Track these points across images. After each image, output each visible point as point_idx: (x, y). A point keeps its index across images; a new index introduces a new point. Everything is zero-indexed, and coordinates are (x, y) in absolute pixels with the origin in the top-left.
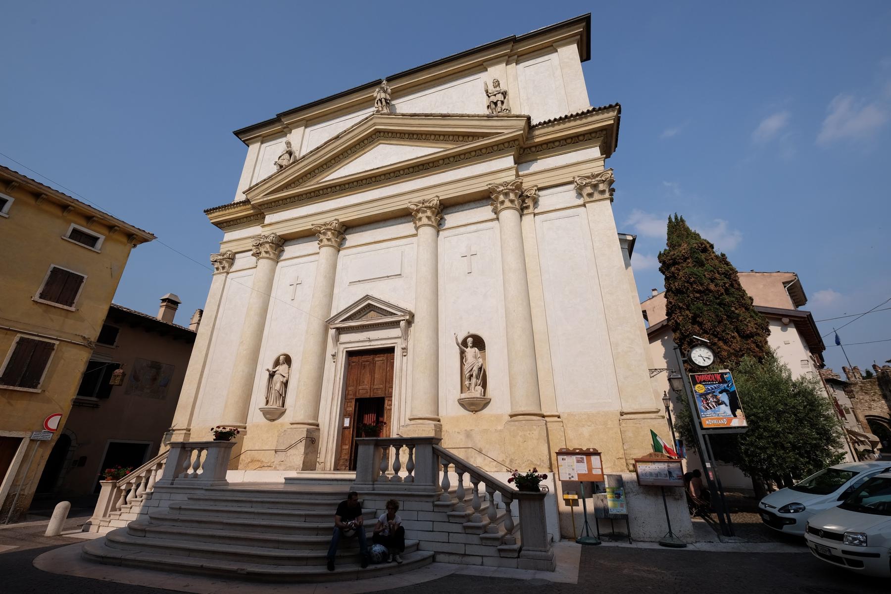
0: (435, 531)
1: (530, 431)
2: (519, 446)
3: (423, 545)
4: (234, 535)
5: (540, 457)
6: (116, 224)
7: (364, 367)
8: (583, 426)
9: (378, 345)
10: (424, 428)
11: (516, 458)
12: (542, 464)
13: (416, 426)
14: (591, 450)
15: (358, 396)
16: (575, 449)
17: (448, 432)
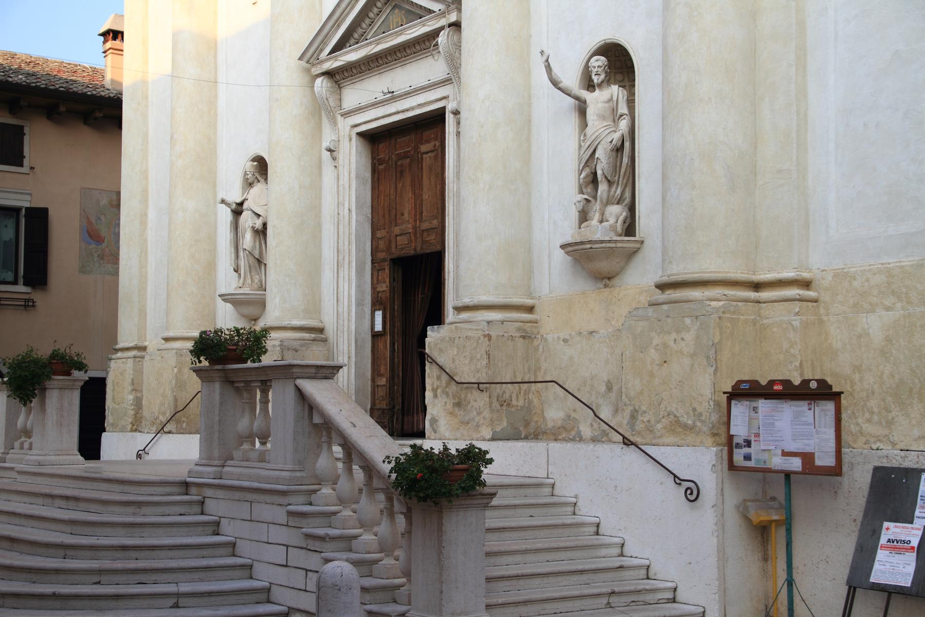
0: (289, 566)
1: (678, 331)
2: (652, 375)
3: (276, 592)
5: (695, 405)
7: (402, 172)
8: (872, 311)
9: (412, 109)
10: (470, 334)
11: (644, 408)
12: (699, 424)
13: (456, 327)
14: (813, 385)
15: (396, 253)
16: (772, 383)
17: (546, 340)
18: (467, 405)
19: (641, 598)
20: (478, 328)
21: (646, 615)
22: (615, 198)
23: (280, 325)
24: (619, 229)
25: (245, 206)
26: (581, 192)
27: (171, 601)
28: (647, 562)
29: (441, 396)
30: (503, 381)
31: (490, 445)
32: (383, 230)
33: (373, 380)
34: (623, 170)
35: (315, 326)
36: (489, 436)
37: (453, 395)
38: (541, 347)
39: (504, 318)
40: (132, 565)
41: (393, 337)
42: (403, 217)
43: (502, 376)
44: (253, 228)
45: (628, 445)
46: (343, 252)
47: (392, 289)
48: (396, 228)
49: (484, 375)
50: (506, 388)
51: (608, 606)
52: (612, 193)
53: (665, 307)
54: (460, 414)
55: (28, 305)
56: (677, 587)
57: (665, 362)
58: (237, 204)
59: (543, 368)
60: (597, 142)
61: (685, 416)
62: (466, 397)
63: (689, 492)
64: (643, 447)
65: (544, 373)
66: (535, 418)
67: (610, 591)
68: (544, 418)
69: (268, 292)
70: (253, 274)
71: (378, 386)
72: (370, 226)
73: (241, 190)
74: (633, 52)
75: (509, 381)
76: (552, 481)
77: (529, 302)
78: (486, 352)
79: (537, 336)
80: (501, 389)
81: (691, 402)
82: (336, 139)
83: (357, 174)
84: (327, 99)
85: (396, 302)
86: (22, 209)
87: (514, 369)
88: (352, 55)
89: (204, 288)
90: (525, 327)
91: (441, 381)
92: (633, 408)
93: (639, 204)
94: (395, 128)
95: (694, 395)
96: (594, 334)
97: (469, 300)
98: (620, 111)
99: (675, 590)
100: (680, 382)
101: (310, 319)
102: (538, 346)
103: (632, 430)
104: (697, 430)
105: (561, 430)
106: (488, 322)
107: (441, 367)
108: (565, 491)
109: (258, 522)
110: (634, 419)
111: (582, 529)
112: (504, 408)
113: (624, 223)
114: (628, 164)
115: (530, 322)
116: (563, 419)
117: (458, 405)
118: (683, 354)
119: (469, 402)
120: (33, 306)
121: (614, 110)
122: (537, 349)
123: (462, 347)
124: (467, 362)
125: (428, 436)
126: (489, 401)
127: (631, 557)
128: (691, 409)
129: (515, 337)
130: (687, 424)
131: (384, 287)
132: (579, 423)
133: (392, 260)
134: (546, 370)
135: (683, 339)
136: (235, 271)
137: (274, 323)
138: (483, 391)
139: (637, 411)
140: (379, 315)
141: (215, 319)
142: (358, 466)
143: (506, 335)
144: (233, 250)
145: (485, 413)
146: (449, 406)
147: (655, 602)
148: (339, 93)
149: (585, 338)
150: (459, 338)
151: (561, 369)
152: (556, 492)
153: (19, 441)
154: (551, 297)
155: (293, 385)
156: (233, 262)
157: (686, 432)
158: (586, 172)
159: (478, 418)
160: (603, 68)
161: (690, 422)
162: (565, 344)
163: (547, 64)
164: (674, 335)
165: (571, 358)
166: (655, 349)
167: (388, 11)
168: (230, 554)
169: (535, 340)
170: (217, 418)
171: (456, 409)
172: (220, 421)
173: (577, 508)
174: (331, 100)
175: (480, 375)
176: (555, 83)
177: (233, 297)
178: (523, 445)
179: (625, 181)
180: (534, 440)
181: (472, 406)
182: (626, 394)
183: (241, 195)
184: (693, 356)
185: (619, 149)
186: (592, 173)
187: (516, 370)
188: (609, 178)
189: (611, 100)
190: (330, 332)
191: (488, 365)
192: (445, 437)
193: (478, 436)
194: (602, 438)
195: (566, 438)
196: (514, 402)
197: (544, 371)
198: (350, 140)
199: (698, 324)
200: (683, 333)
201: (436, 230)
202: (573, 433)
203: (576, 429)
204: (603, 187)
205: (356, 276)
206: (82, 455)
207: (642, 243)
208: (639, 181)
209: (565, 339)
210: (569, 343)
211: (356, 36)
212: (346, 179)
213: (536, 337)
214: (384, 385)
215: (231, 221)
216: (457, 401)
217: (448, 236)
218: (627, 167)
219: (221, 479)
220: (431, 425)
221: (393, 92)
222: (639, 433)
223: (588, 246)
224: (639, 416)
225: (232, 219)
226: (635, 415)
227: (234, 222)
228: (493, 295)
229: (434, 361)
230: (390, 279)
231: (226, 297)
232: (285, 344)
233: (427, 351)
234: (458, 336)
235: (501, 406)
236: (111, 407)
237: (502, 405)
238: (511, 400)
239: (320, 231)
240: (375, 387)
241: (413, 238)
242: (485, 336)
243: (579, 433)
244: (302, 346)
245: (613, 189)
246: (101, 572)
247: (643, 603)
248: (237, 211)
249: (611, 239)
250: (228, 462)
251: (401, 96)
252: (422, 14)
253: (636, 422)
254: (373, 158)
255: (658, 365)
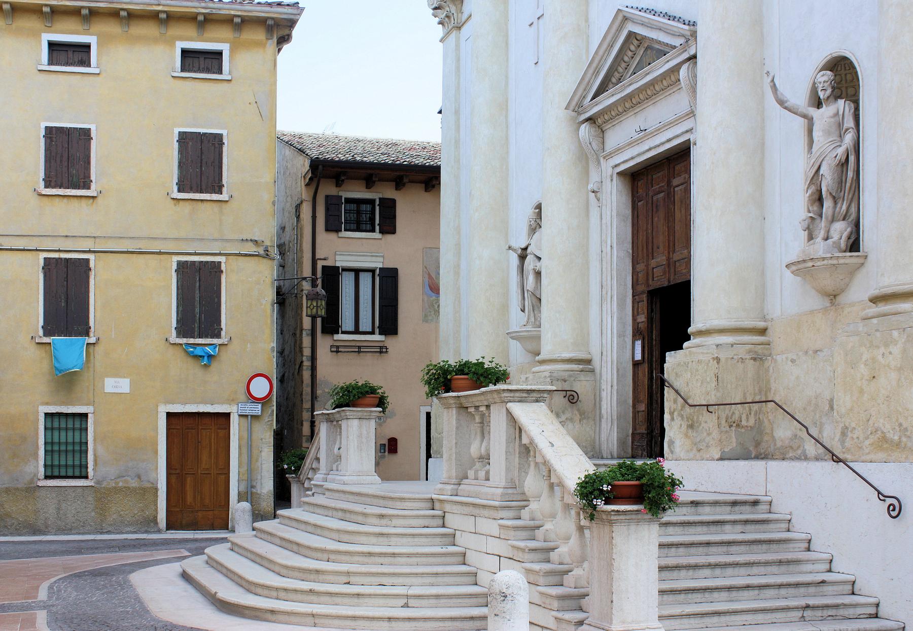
1: (886, 345)
4: (756, 606)
5: (901, 420)
6: (233, 13)
10: (701, 357)
11: (853, 425)
18: (698, 427)
19: (842, 612)
20: (708, 351)
21: (850, 628)
22: (841, 214)
23: (552, 358)
24: (843, 245)
25: (529, 251)
26: (809, 212)
27: (402, 601)
28: (852, 578)
29: (677, 419)
30: (733, 402)
31: (717, 464)
32: (642, 264)
33: (634, 406)
34: (848, 185)
35: (583, 358)
36: (718, 456)
37: (687, 418)
38: (771, 368)
39: (734, 341)
40: (374, 569)
41: (652, 365)
42: (658, 250)
43: (731, 398)
44: (534, 270)
45: (838, 462)
46: (606, 287)
47: (650, 320)
48: (653, 261)
49: (713, 397)
50: (735, 410)
51: (802, 619)
52: (838, 209)
53: (875, 321)
54: (693, 436)
55: (382, 350)
56: (879, 602)
57: (874, 377)
58: (522, 249)
59: (773, 389)
60: (822, 159)
61: (891, 431)
62: (698, 418)
63: (891, 508)
64: (851, 464)
65: (774, 394)
66: (766, 438)
67: (804, 605)
68: (773, 437)
69: (542, 329)
70: (536, 312)
71: (638, 412)
72: (631, 261)
73: (527, 236)
74: (858, 63)
75: (739, 402)
76: (769, 499)
77: (761, 324)
78: (715, 375)
79: (768, 358)
80: (730, 410)
81: (897, 417)
82: (600, 181)
83: (618, 212)
84: (590, 144)
85: (654, 332)
86: (376, 269)
87: (745, 390)
88: (607, 100)
89: (498, 328)
90: (756, 350)
91: (677, 404)
92: (843, 425)
93: (863, 219)
94: (651, 165)
95: (900, 410)
96: (819, 353)
97: (702, 325)
98: (846, 125)
99: (877, 605)
100: (887, 397)
101: (580, 351)
102: (768, 367)
103: (842, 447)
104: (903, 446)
105: (788, 449)
106: (717, 346)
107: (677, 391)
108: (782, 508)
109: (480, 534)
110: (844, 436)
111: (791, 545)
112: (733, 429)
113: (849, 238)
114: (853, 178)
115: (762, 344)
116: (791, 439)
117: (691, 426)
118: (891, 369)
119: (700, 424)
120: (387, 352)
121: (840, 125)
122: (767, 370)
123: (694, 371)
124: (699, 384)
125: (666, 457)
126: (718, 422)
127: (839, 573)
128: (897, 424)
129: (746, 359)
130: (894, 439)
131: (642, 318)
132: (804, 442)
133: (649, 292)
134: (775, 390)
135: (890, 353)
136: (522, 310)
137: (546, 356)
138: (712, 412)
139: (847, 428)
140: (639, 344)
141: (508, 356)
142: (334, 465)
143: (735, 357)
144: (520, 291)
145: (714, 434)
146: (684, 427)
147: (855, 617)
148: (602, 136)
149: (810, 357)
150: (692, 362)
151: (789, 389)
152: (773, 509)
153: (336, 464)
154: (782, 318)
155: (504, 410)
156: (520, 303)
157: (893, 448)
158: (811, 190)
159: (709, 438)
160: (829, 83)
161: (896, 438)
162: (792, 365)
163: (772, 84)
164: (882, 350)
165: (798, 378)
166: (865, 364)
167: (641, 52)
168: (461, 563)
169: (766, 361)
170: (454, 441)
171: (690, 431)
172: (456, 443)
173: (791, 525)
174: (594, 144)
175: (709, 397)
176: (782, 103)
177: (518, 334)
178: (745, 464)
179: (850, 196)
180: (756, 460)
181: (703, 427)
182: (838, 412)
183: (527, 239)
184: (900, 369)
185: (844, 164)
186: (817, 190)
187: (746, 391)
188: (834, 194)
189: (837, 114)
190: (596, 363)
191: (717, 388)
192: (680, 457)
193: (708, 456)
194: (825, 456)
195: (793, 457)
196: (744, 423)
197: (773, 391)
198: (612, 180)
199: (905, 337)
200: (891, 347)
201: (686, 259)
202: (799, 452)
203: (802, 448)
204: (828, 204)
205: (618, 309)
206: (379, 476)
207: (866, 258)
208: (863, 195)
209: (793, 359)
210: (796, 363)
211: (614, 80)
212: (609, 218)
213: (766, 359)
214: (643, 411)
215: (518, 265)
216: (690, 423)
217: (693, 265)
218: (852, 181)
219: (457, 496)
220: (669, 446)
221: (646, 130)
222: (849, 450)
223: (810, 264)
224: (849, 433)
225: (519, 264)
226: (846, 432)
227: (521, 266)
228: (725, 319)
229: (671, 386)
230: (647, 310)
231: (512, 335)
232: (555, 375)
233: (666, 376)
234: (692, 360)
235: (730, 428)
236: (434, 437)
237: (731, 426)
238: (741, 421)
239: (588, 268)
240: (635, 413)
241: (667, 269)
242: (713, 359)
243: (804, 451)
244: (570, 376)
245: (839, 205)
246: (350, 574)
247: (841, 618)
248: (523, 257)
249: (832, 256)
250: (464, 480)
251: (652, 133)
252: (666, 50)
253: (846, 439)
254: (633, 196)
255: (867, 380)
